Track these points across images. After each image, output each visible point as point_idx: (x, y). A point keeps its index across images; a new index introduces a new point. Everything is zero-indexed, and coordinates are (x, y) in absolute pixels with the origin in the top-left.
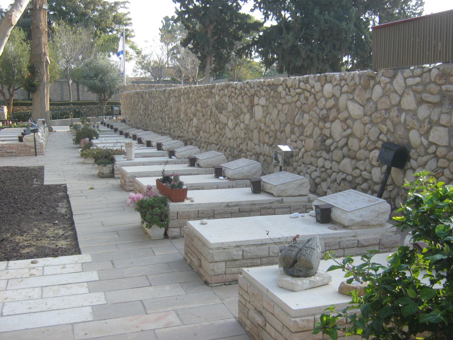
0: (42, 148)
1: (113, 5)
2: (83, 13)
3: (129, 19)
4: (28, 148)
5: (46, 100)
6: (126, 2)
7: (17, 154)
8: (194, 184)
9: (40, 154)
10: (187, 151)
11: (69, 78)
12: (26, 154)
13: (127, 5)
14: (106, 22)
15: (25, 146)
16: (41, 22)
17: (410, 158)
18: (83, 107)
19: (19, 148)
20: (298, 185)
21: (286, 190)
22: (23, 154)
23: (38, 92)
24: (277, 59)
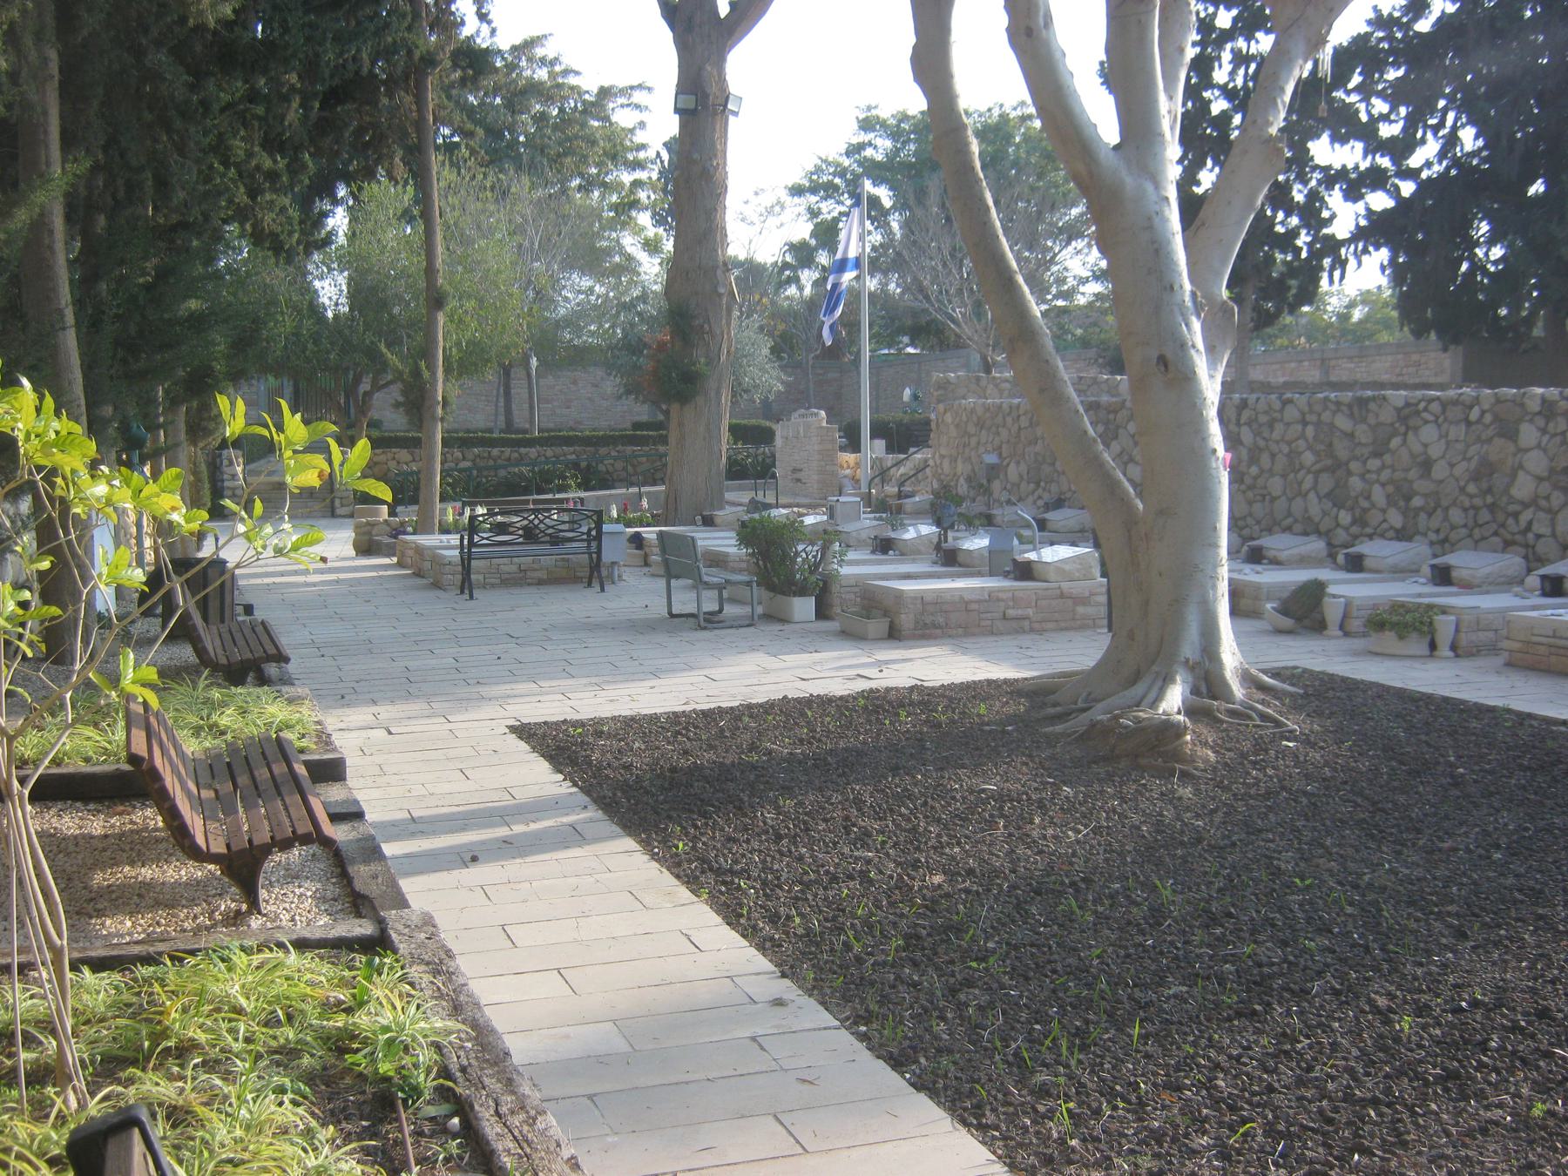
4: (1070, 602)
6: (640, 87)
7: (1036, 626)
15: (1062, 596)
18: (603, 451)
19: (1044, 603)
23: (700, 400)
24: (1477, 244)
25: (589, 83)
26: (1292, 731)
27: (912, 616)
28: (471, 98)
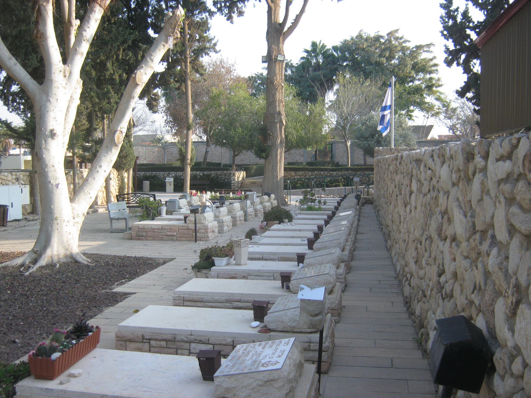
0: (207, 232)
1: (415, 49)
2: (376, 61)
3: (436, 65)
5: (278, 168)
7: (178, 238)
8: (195, 331)
9: (204, 239)
10: (318, 258)
11: (348, 138)
12: (188, 239)
13: (432, 48)
14: (403, 71)
15: (188, 229)
16: (276, 76)
17: (493, 369)
20: (260, 383)
21: (234, 388)
22: (185, 239)
25: (411, 45)
26: (46, 269)
27: (135, 232)
28: (465, 43)
